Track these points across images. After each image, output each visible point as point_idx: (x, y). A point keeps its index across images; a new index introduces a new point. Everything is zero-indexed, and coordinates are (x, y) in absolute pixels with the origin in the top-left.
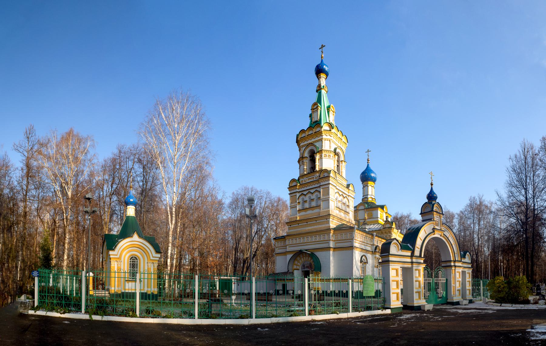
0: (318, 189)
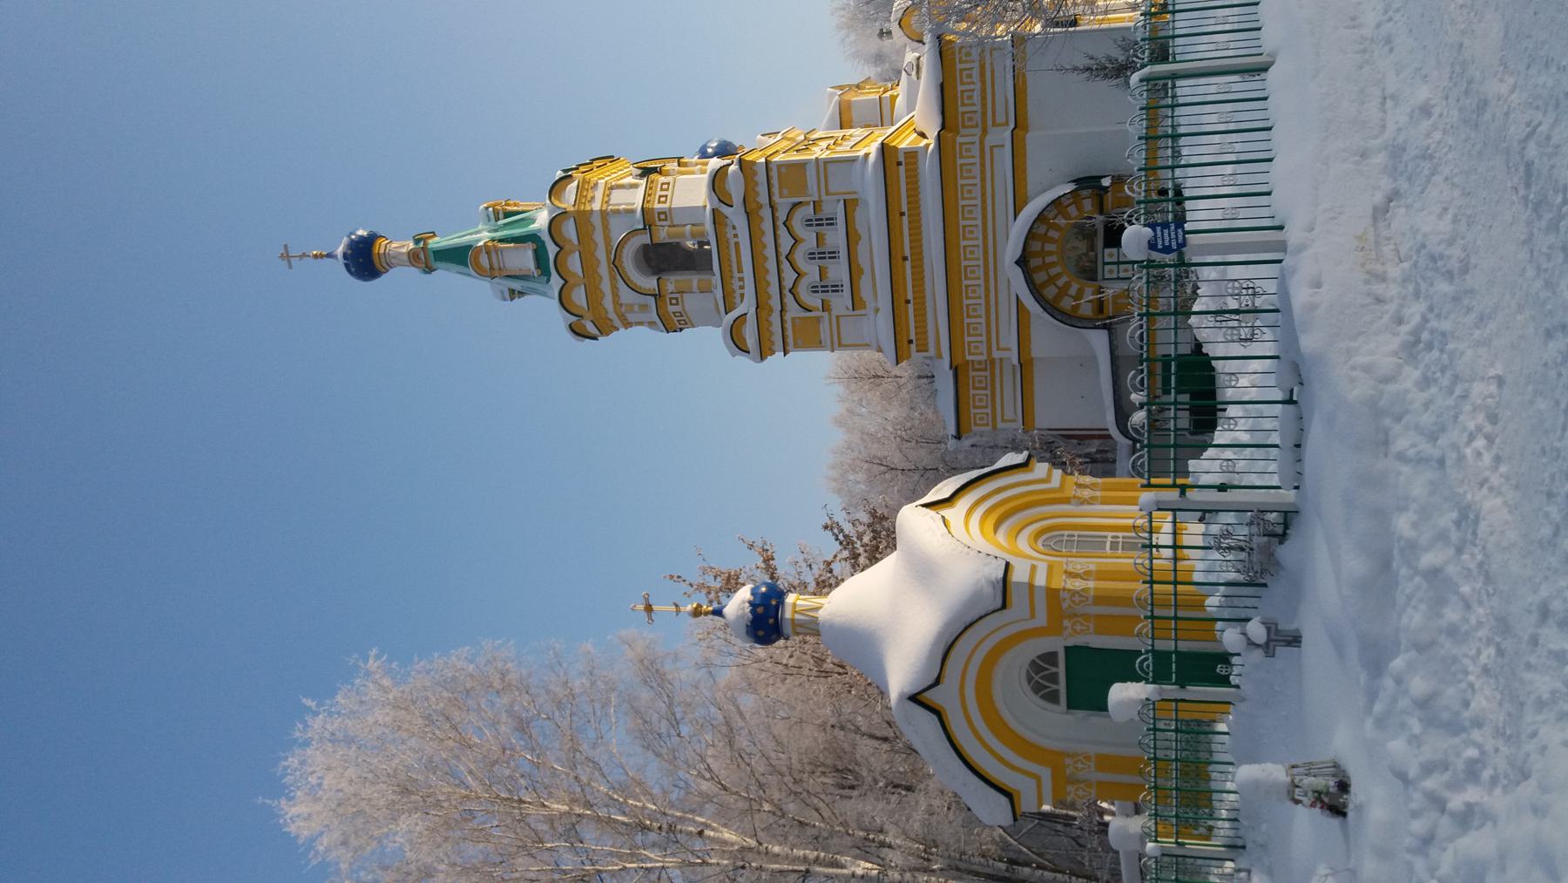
0: (782, 215)
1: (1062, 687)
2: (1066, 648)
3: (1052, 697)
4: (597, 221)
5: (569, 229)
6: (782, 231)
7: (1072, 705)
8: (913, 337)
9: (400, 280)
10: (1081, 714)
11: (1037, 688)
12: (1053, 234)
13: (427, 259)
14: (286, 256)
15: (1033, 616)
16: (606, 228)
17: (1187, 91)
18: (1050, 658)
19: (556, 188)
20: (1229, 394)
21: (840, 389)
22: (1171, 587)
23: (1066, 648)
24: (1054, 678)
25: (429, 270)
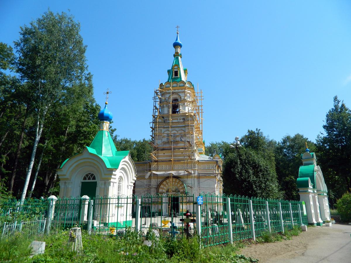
1: (87, 181)
2: (96, 182)
3: (85, 179)
4: (183, 90)
5: (182, 85)
6: (180, 129)
7: (82, 183)
8: (165, 154)
9: (173, 51)
10: (81, 185)
11: (87, 175)
12: (176, 184)
13: (176, 55)
14: (178, 27)
15: (105, 174)
16: (182, 92)
17: (97, 206)
18: (94, 178)
19: (190, 83)
20: (152, 218)
21: (294, 136)
22: (109, 203)
23: (96, 182)
24: (89, 179)
25: (174, 56)
